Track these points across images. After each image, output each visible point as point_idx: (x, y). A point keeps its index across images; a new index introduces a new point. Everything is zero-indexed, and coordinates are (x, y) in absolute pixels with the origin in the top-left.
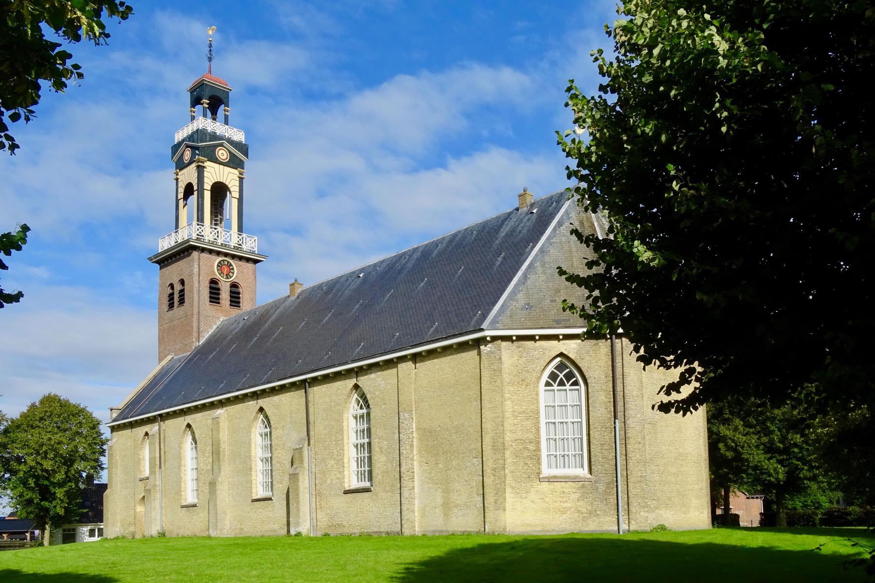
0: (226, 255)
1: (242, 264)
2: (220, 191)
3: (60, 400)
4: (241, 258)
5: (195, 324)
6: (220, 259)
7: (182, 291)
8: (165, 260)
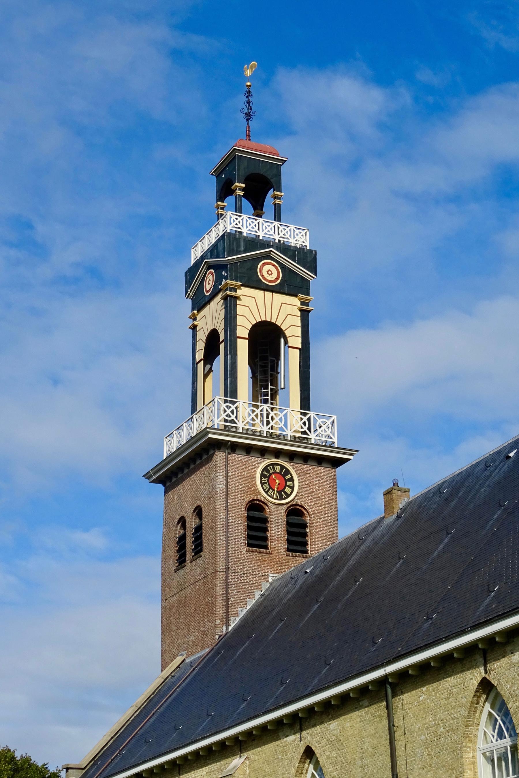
0: (278, 453)
1: (311, 468)
2: (266, 339)
3: (13, 758)
4: (306, 458)
5: (220, 590)
6: (266, 462)
7: (199, 529)
8: (171, 474)
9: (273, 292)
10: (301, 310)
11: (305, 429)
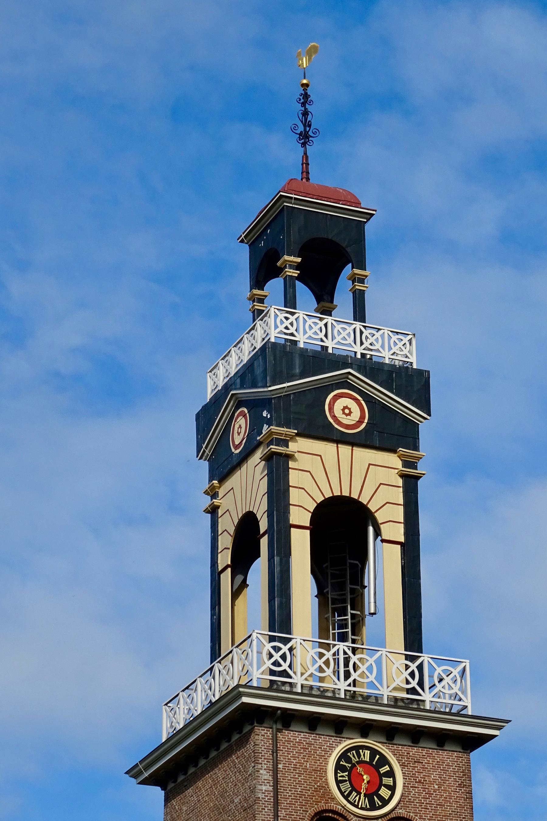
9: (353, 444)
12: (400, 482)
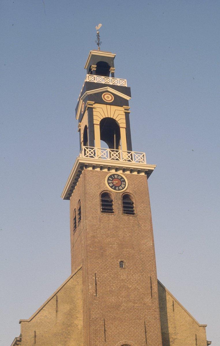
9: (110, 105)
10: (125, 113)
11: (130, 159)
12: (124, 114)
